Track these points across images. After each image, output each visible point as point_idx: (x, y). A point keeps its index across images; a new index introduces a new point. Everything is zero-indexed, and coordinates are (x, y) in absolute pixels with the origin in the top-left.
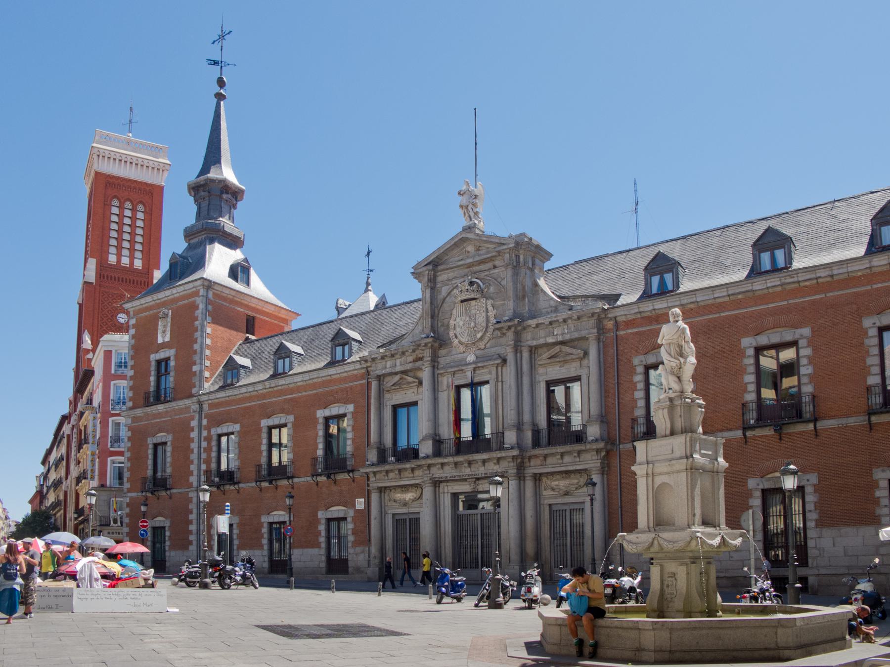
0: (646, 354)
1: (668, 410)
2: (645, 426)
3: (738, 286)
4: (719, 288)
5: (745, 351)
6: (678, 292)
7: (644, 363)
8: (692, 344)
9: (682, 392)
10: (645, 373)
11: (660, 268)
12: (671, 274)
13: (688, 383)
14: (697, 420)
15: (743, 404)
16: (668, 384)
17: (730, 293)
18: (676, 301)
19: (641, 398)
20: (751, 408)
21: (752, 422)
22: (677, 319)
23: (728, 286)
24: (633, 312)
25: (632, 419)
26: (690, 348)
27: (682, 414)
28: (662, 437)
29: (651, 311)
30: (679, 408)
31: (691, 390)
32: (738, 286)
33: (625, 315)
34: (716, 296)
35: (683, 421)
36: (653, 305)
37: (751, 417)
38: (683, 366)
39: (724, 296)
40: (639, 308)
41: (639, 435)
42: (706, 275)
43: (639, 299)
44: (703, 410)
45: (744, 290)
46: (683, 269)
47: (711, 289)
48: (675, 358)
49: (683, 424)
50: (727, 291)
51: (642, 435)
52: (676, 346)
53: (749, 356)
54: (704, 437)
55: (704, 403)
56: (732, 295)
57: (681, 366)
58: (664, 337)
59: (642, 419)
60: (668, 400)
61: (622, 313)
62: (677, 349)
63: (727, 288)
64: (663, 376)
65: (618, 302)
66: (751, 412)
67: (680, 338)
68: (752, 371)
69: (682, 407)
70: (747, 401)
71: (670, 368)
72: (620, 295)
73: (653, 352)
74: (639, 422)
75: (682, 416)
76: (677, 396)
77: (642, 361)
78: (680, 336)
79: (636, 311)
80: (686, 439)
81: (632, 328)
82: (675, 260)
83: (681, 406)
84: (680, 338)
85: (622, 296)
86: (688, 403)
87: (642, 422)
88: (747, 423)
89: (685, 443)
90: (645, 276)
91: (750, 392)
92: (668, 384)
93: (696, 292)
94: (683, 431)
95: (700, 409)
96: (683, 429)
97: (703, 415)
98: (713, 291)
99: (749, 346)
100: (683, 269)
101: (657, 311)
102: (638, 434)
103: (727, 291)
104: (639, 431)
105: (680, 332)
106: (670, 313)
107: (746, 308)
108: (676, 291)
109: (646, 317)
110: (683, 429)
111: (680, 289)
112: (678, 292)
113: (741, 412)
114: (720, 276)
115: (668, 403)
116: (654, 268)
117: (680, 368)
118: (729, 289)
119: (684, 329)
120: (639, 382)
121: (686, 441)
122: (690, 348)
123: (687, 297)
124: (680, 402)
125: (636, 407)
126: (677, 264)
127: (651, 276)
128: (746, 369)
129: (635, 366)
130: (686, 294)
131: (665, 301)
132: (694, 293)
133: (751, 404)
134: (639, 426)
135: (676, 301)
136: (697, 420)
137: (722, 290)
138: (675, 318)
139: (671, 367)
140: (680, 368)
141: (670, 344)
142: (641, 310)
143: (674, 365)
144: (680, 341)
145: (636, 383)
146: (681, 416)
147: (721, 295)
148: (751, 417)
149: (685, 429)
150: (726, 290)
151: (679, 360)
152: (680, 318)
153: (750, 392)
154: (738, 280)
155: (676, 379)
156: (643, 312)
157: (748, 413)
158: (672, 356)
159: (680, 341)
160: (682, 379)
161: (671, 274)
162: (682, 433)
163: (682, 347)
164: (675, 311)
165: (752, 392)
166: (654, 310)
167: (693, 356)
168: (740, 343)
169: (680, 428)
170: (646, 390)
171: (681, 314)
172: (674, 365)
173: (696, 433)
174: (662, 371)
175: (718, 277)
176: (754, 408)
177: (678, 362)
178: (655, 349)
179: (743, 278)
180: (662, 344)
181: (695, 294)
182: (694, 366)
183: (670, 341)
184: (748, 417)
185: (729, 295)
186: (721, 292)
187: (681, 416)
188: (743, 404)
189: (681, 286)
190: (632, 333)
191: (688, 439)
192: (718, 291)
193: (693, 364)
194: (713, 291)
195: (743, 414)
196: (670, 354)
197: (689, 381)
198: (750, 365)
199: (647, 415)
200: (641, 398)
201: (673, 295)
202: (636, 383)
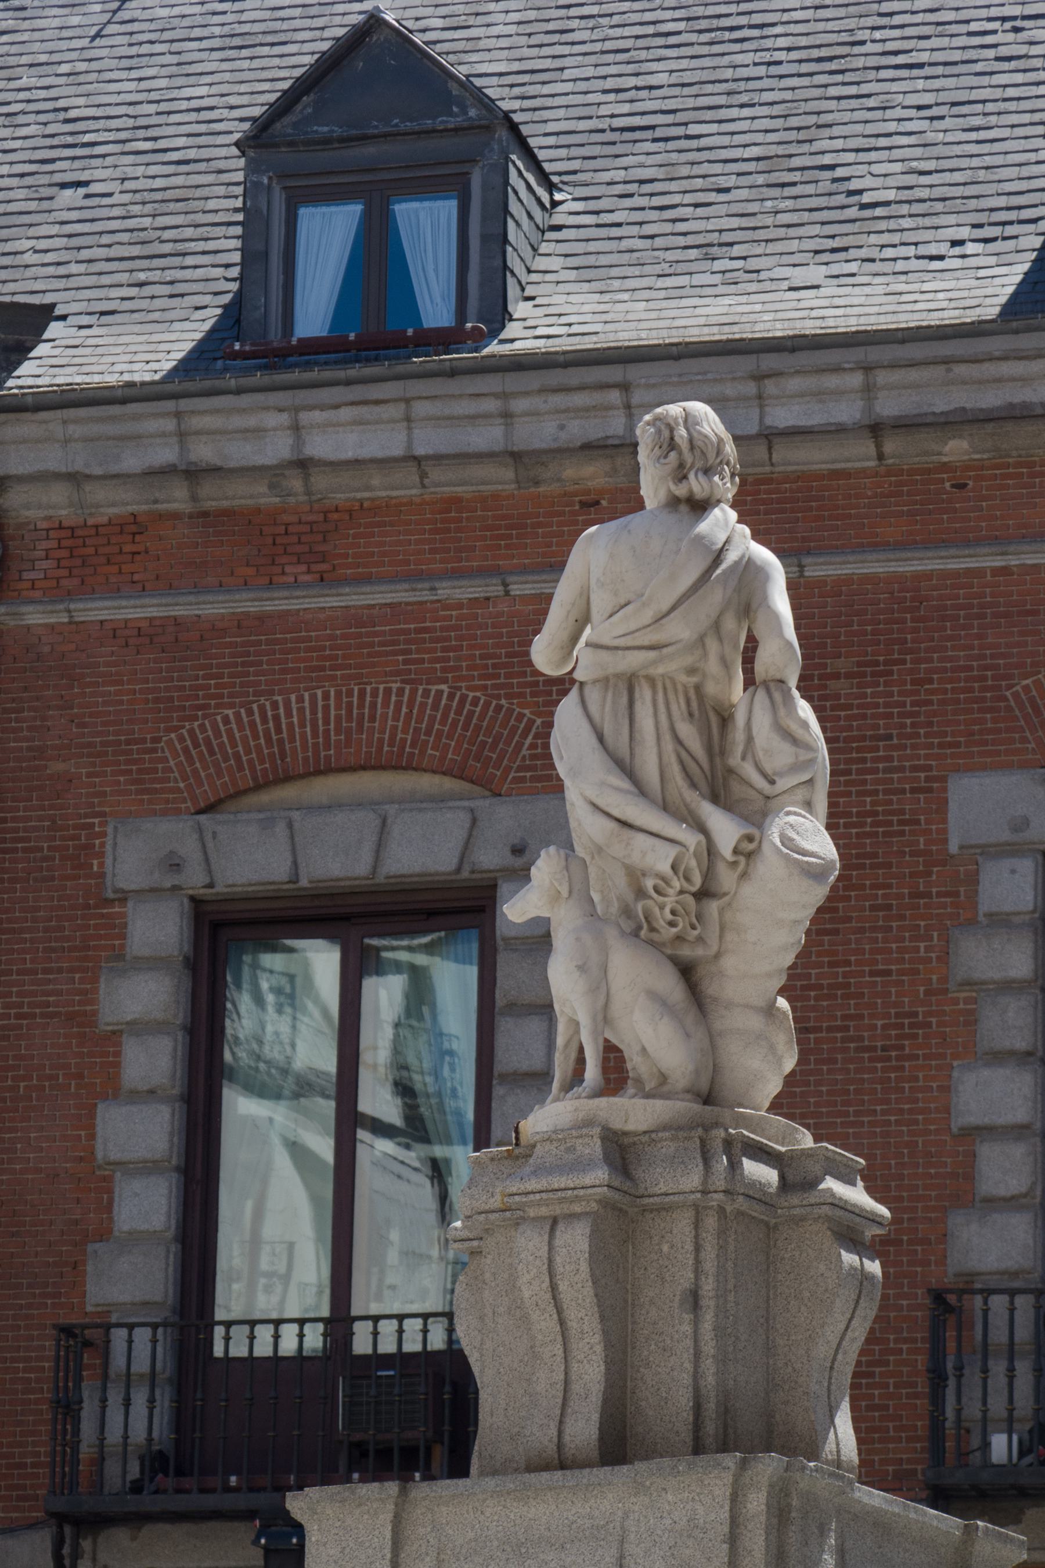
0: (209, 809)
1: (595, 1236)
2: (165, 1399)
3: (947, 361)
4: (804, 359)
5: (973, 879)
6: (494, 348)
7: (194, 879)
8: (805, 709)
9: (708, 1099)
10: (192, 965)
11: (369, 151)
12: (447, 208)
13: (755, 1022)
14: (823, 1350)
15: (938, 1297)
16: (604, 1016)
17: (888, 407)
18: (473, 418)
19: (148, 1168)
20: (999, 1335)
21: (1000, 1447)
22: (697, 485)
23: (874, 354)
24: (132, 462)
25: (67, 1331)
26: (795, 741)
27: (708, 1287)
28: (538, 1465)
29: (273, 473)
30: (682, 1225)
31: (773, 1087)
32: (947, 361)
33: (75, 479)
34: (782, 417)
35: (709, 1347)
36: (296, 428)
37: (997, 1405)
38: (726, 878)
39: (839, 430)
40: (182, 435)
41: (112, 1469)
42: (707, 251)
43: (186, 367)
44: (874, 1267)
45: (990, 399)
46: (544, 178)
47: (746, 364)
48: (666, 807)
49: (709, 1367)
50: (868, 390)
51: (134, 1471)
52: (678, 709)
53: (1000, 921)
54: (873, 1498)
55: (883, 1211)
56: (906, 425)
57: (709, 874)
58: (584, 620)
59: (142, 1335)
60: (595, 1148)
61: (53, 460)
62: (688, 732)
63: (868, 369)
64: (561, 940)
65: (27, 368)
66: (998, 1368)
67: (713, 646)
68: (1021, 1044)
69: (711, 1222)
70: (972, 1276)
71: (621, 882)
72: (46, 314)
73: (264, 797)
74: (118, 1361)
75: (708, 1303)
76: (673, 1128)
77: (175, 866)
78: (717, 626)
79: (166, 455)
80: (736, 1499)
81: (116, 592)
82: (487, 104)
83: (698, 1212)
84: (713, 646)
85: (54, 329)
86: (755, 1193)
87: (141, 1364)
88: (963, 1454)
89: (733, 1539)
90: (251, 190)
91: (994, 1203)
92: (604, 1016)
93: (635, 373)
94: (710, 1428)
95: (849, 1258)
96: (711, 1407)
97: (868, 1311)
98: (759, 377)
99: (1006, 836)
100: (544, 178)
101: (321, 482)
102: (100, 1460)
103: (868, 390)
104: (114, 1435)
105: (715, 597)
106: (644, 432)
107: (998, 540)
108: (480, 338)
109: (228, 513)
110: (711, 1407)
111: (512, 330)
112: (494, 348)
113: (922, 1361)
114: (815, 273)
115: (600, 1175)
116: (326, 142)
117: (703, 894)
118: (882, 377)
119: (749, 568)
120: (140, 1028)
121: (734, 1521)
122: (795, 741)
123: (558, 400)
124: (692, 1180)
125: (104, 1233)
126: (503, 134)
127: (295, 201)
128: (971, 1020)
129: (123, 897)
130: (555, 377)
131: (395, 411)
132: (613, 373)
133: (998, 1302)
134: (115, 1398)
135: (473, 418)
136: (823, 1350)
137: (832, 381)
138: (681, 475)
139: (635, 876)
140: (703, 894)
141: (630, 683)
142: (203, 452)
143: (661, 859)
144: (713, 666)
145: (114, 1037)
146: (694, 1300)
147: (814, 416)
148: (997, 1405)
149: (726, 1411)
150: (856, 380)
151: (701, 828)
152: (726, 486)
153: (994, 1203)
154: (950, 317)
155: (670, 984)
156: (215, 470)
157: (972, 1377)
158: (641, 789)
159: (713, 666)
160: (711, 988)
161: (447, 208)
162: (698, 1449)
163: (725, 719)
164: (688, 419)
165: (1011, 1203)
166: (303, 465)
167: (808, 805)
168: (943, 805)
169: (684, 1400)
170: (188, 1099)
171: (730, 449)
172: (661, 859)
173: (814, 1454)
174: (555, 898)
175: (799, 275)
176: (1024, 1332)
177: (691, 839)
178: (288, 778)
179: (991, 311)
180: (563, 685)
181: (625, 387)
182: (819, 894)
183: (634, 660)
184: (973, 1410)
185: (876, 429)
186: (820, 395)
187: (694, 1300)
188: (938, 1297)
189: (520, 309)
190: (113, 632)
191: (756, 1503)
192: (794, 384)
193: (815, 873)
194: (759, 377)
195: (937, 1378)
196: (627, 768)
197: (770, 1011)
198: (1008, 986)
199: (182, 1307)
200: (148, 1168)
201: (453, 372)
202: (114, 1037)
